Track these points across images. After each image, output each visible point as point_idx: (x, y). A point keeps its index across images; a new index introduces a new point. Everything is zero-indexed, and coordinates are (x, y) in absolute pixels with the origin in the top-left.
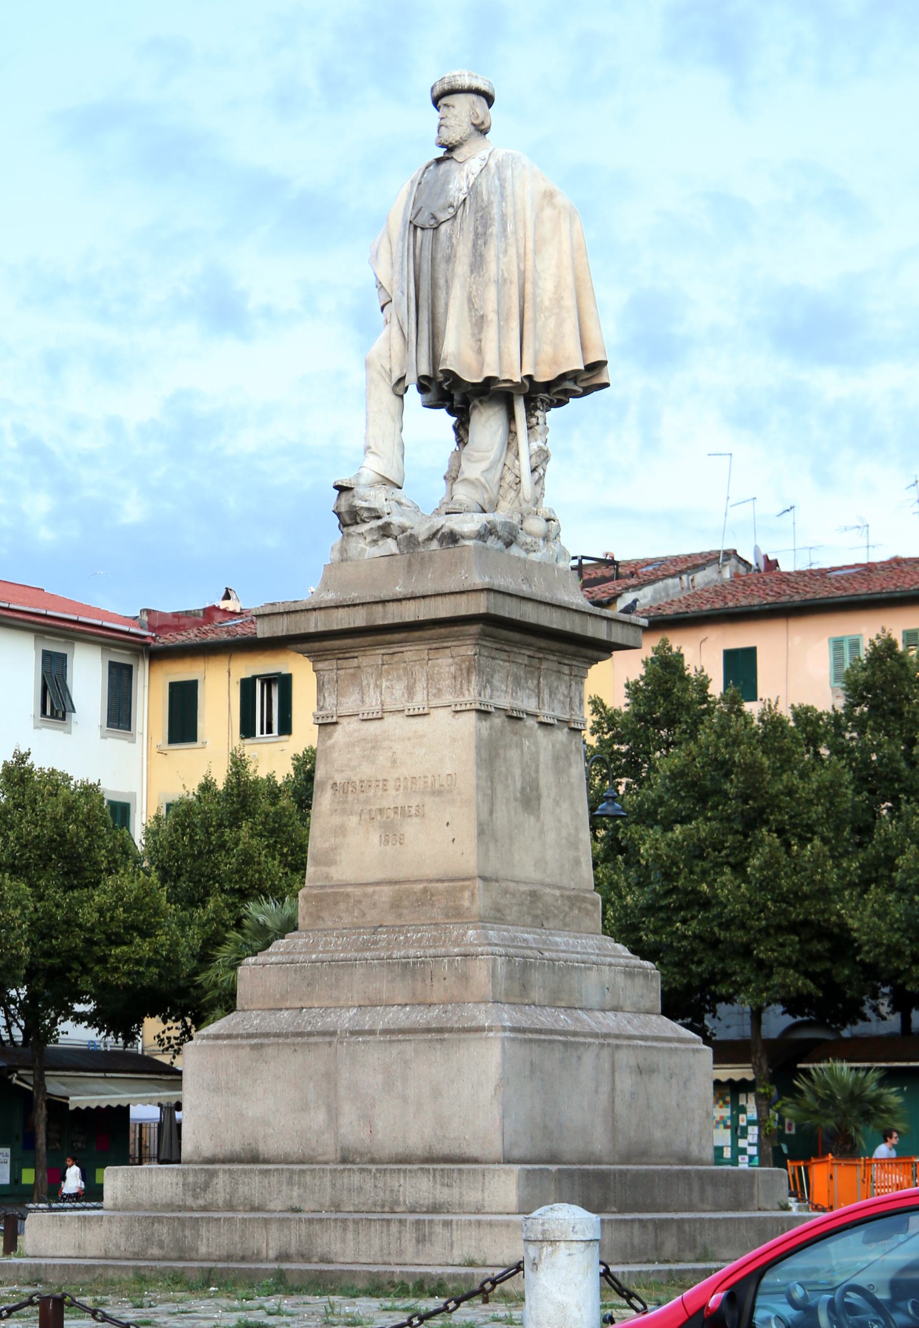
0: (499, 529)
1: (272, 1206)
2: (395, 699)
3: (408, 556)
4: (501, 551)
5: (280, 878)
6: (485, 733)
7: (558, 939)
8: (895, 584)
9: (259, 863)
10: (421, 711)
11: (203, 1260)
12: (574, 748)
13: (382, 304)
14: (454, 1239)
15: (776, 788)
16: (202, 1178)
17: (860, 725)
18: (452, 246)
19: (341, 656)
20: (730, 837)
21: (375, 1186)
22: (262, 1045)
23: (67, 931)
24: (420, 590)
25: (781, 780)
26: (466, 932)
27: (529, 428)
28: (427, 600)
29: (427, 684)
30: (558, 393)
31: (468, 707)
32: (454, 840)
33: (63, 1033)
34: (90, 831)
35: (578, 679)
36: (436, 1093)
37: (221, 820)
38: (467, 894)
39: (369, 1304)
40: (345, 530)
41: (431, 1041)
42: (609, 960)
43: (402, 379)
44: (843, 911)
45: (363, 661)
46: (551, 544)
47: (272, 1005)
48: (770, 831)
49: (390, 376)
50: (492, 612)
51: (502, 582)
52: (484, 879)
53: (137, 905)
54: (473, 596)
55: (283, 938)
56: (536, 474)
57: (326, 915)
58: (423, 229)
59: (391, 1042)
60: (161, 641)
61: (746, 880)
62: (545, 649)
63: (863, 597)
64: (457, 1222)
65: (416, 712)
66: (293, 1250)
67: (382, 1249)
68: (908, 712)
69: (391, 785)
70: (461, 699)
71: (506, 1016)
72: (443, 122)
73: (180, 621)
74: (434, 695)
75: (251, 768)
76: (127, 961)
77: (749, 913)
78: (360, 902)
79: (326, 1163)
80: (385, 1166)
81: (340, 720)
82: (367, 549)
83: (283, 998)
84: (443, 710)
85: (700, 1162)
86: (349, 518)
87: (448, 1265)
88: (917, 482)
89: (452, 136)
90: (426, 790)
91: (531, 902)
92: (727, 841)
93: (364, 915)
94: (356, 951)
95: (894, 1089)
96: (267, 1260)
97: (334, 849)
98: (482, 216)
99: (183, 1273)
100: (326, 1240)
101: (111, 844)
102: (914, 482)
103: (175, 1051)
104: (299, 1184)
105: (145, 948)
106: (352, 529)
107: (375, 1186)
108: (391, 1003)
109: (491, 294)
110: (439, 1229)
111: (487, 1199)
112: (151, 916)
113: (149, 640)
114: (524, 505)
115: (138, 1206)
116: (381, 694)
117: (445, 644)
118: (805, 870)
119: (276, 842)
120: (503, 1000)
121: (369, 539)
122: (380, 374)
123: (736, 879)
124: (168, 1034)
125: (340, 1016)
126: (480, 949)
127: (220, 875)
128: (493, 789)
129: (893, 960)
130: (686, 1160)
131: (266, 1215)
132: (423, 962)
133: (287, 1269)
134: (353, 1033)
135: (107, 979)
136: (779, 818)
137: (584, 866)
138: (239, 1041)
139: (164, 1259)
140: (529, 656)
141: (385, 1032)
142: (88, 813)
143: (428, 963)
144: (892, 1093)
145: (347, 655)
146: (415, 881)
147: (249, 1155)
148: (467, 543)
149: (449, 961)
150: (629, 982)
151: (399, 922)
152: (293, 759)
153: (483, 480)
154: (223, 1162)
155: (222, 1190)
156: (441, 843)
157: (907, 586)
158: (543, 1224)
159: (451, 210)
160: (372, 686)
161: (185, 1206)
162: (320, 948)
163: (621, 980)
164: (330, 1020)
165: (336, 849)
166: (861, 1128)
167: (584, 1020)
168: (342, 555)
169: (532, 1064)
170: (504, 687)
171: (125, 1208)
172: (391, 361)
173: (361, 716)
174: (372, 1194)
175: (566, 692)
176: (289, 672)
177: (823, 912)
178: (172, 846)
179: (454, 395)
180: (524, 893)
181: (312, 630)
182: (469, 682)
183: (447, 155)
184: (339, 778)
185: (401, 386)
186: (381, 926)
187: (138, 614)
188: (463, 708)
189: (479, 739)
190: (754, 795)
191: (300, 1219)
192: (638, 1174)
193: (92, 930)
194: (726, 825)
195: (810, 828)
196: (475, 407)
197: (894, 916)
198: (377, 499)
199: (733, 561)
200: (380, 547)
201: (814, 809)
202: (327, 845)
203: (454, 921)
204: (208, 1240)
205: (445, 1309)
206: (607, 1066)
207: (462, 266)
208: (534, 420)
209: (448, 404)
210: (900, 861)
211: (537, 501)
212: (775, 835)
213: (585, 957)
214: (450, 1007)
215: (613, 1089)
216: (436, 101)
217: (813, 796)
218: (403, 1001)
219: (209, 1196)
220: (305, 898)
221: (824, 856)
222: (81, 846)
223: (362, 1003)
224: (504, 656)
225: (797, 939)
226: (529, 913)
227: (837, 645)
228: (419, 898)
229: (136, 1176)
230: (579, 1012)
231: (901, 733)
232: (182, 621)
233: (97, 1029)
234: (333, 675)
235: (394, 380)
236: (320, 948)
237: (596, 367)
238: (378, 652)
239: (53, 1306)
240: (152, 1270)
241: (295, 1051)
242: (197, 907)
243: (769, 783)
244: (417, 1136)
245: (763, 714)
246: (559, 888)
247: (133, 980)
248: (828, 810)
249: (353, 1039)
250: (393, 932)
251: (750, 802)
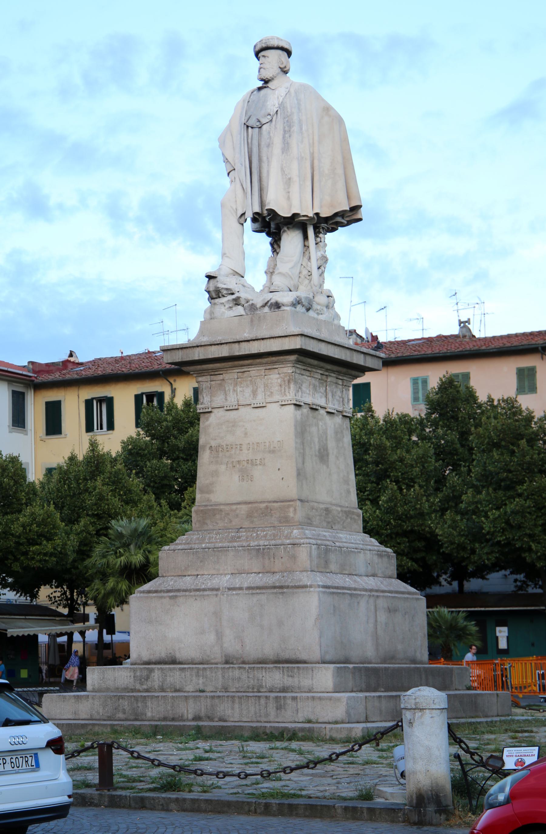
0: (303, 301)
1: (187, 689)
2: (246, 398)
3: (251, 316)
4: (304, 313)
5: (119, 508)
6: (299, 417)
7: (341, 535)
8: (446, 349)
9: (108, 500)
10: (261, 405)
11: (149, 720)
12: (345, 427)
13: (228, 171)
14: (299, 707)
15: (394, 458)
16: (145, 673)
17: (435, 424)
18: (270, 138)
19: (213, 373)
20: (369, 485)
21: (248, 677)
22: (176, 597)
23: (5, 538)
24: (260, 335)
25: (396, 454)
26: (292, 531)
27: (316, 244)
30: (333, 224)
31: (289, 402)
32: (283, 479)
33: (3, 594)
34: (16, 482)
35: (347, 387)
36: (280, 623)
37: (85, 476)
38: (291, 509)
39: (259, 745)
40: (213, 301)
41: (276, 593)
42: (369, 547)
43: (244, 214)
44: (432, 525)
45: (226, 376)
46: (330, 310)
47: (180, 573)
48: (391, 481)
49: (236, 213)
50: (304, 348)
51: (308, 331)
52: (301, 501)
53: (44, 523)
54: (293, 338)
55: (184, 535)
56: (320, 270)
57: (208, 522)
58: (252, 128)
59: (252, 594)
60: (40, 379)
61: (379, 508)
62: (330, 370)
63: (429, 356)
64: (300, 697)
65: (258, 405)
66: (203, 714)
67: (256, 713)
68: (462, 417)
69: (244, 447)
70: (285, 398)
71: (318, 579)
72: (262, 66)
73: (50, 367)
74: (269, 396)
75: (100, 447)
76: (39, 554)
77: (381, 526)
78: (228, 514)
79: (216, 664)
80: (253, 666)
81: (213, 410)
82: (225, 311)
83: (186, 569)
84: (274, 404)
85: (421, 663)
86: (215, 295)
87: (295, 722)
88: (456, 293)
89: (267, 75)
90: (269, 449)
91: (326, 514)
92: (367, 487)
93: (231, 521)
94: (228, 542)
95: (473, 623)
96: (188, 720)
97: (212, 484)
98: (287, 121)
99: (140, 728)
100: (222, 708)
101: (27, 489)
102: (454, 294)
103: (58, 604)
104: (203, 676)
105: (48, 547)
106: (217, 301)
107: (248, 677)
108: (250, 572)
109: (295, 166)
110: (289, 702)
111: (315, 684)
112: (52, 529)
113: (33, 379)
114: (314, 288)
115: (108, 689)
117: (275, 367)
118: (411, 502)
119: (116, 488)
120: (316, 570)
121: (227, 306)
123: (373, 507)
124: (54, 594)
125: (221, 579)
126: (302, 541)
127: (86, 506)
128: (304, 449)
129: (461, 552)
130: (414, 661)
131: (186, 694)
132: (269, 548)
133: (202, 725)
134: (229, 589)
135: (28, 564)
136: (396, 474)
137: (352, 494)
138: (162, 594)
139: (126, 720)
140: (321, 374)
141: (249, 588)
142: (14, 472)
143: (272, 549)
144: (472, 625)
145: (216, 373)
146: (261, 502)
147: (170, 660)
148: (285, 308)
149: (284, 548)
150: (380, 560)
151: (252, 526)
152: (122, 443)
153: (290, 273)
154: (155, 663)
155: (157, 680)
156: (275, 480)
157: (453, 350)
158: (415, 699)
159: (269, 117)
160: (231, 391)
161: (135, 689)
162: (207, 541)
163: (376, 558)
164: (215, 582)
165: (213, 484)
166: (457, 644)
167: (359, 582)
168: (211, 315)
169: (334, 607)
170: (308, 392)
171: (100, 690)
172: (236, 204)
173: (225, 408)
174: (247, 682)
175: (340, 395)
176: (112, 396)
177: (422, 525)
178: (58, 490)
179: (271, 224)
180: (322, 509)
181: (196, 358)
182: (289, 388)
183: (265, 85)
184: (213, 443)
185: (243, 218)
186: (241, 528)
187: (26, 364)
188: (286, 403)
189: (296, 421)
190: (382, 462)
191: (207, 696)
192: (394, 669)
193: (19, 537)
194: (367, 478)
195: (413, 480)
196: (284, 231)
197: (461, 528)
198: (230, 283)
199: (354, 336)
201: (414, 469)
202: (208, 482)
203: (285, 525)
204: (152, 708)
205: (352, 750)
206: (372, 608)
207: (277, 149)
208: (318, 239)
209: (267, 230)
210: (464, 497)
211: (321, 286)
212: (394, 484)
213: (357, 545)
214: (285, 574)
215: (376, 621)
216: (257, 54)
217: (414, 463)
218: (257, 571)
219: (149, 683)
220: (196, 512)
221: (421, 495)
222: (11, 490)
223: (233, 572)
224: (308, 373)
225: (407, 540)
226: (325, 521)
227: (415, 381)
228: (264, 511)
229: (105, 672)
230: (355, 577)
231: (458, 429)
232: (51, 368)
233: (15, 592)
234: (208, 384)
235: (239, 215)
236: (207, 541)
237: (356, 209)
238: (235, 371)
239: (107, 749)
240: (121, 726)
241: (196, 599)
242: (74, 524)
243: (389, 455)
244: (270, 649)
245: (385, 418)
246: (340, 506)
247: (42, 564)
248: (421, 470)
249: (230, 592)
250: (249, 531)
251: (380, 466)
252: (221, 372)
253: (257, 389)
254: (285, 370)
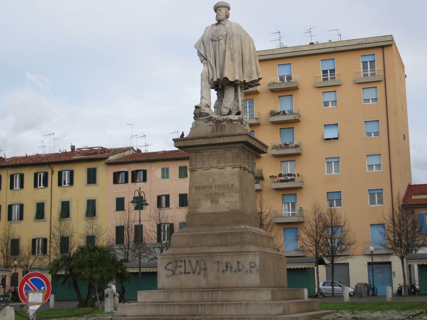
45: (204, 154)
69: (213, 186)
121: (205, 121)
182: (237, 159)
196: (227, 89)
254: (235, 151)
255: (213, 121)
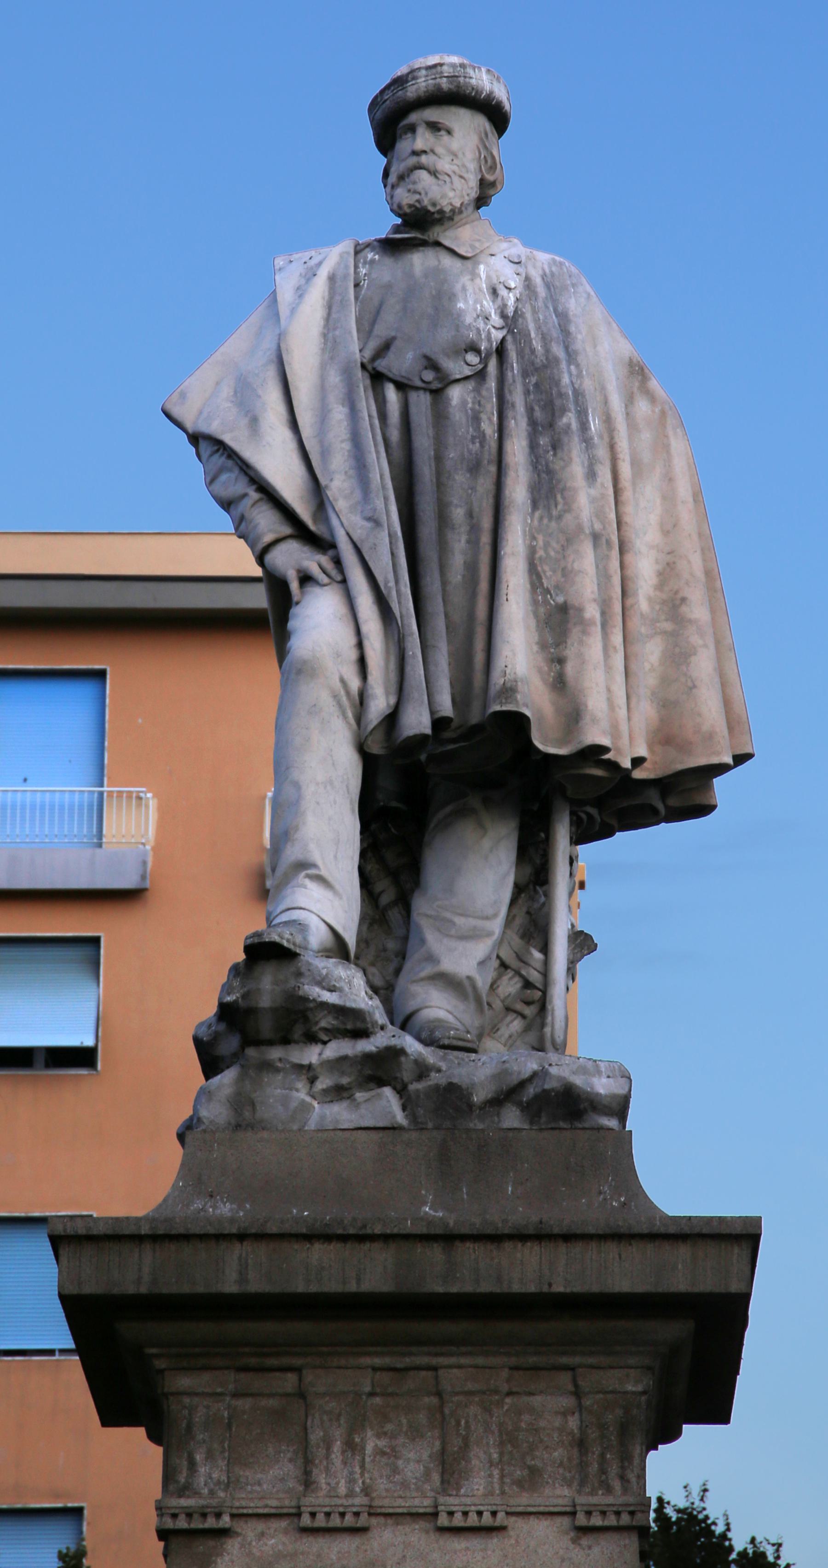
28: (577, 1248)
29: (501, 1454)
45: (318, 1381)
70: (600, 1499)
74: (519, 1483)
98: (537, 385)
116: (363, 1466)
117: (564, 1360)
121: (323, 1083)
122: (335, 697)
159: (472, 358)
160: (337, 1446)
181: (230, 1286)
200: (357, 1106)
252: (297, 1362)
253: (466, 1445)
254: (612, 1380)
255: (401, 1091)
